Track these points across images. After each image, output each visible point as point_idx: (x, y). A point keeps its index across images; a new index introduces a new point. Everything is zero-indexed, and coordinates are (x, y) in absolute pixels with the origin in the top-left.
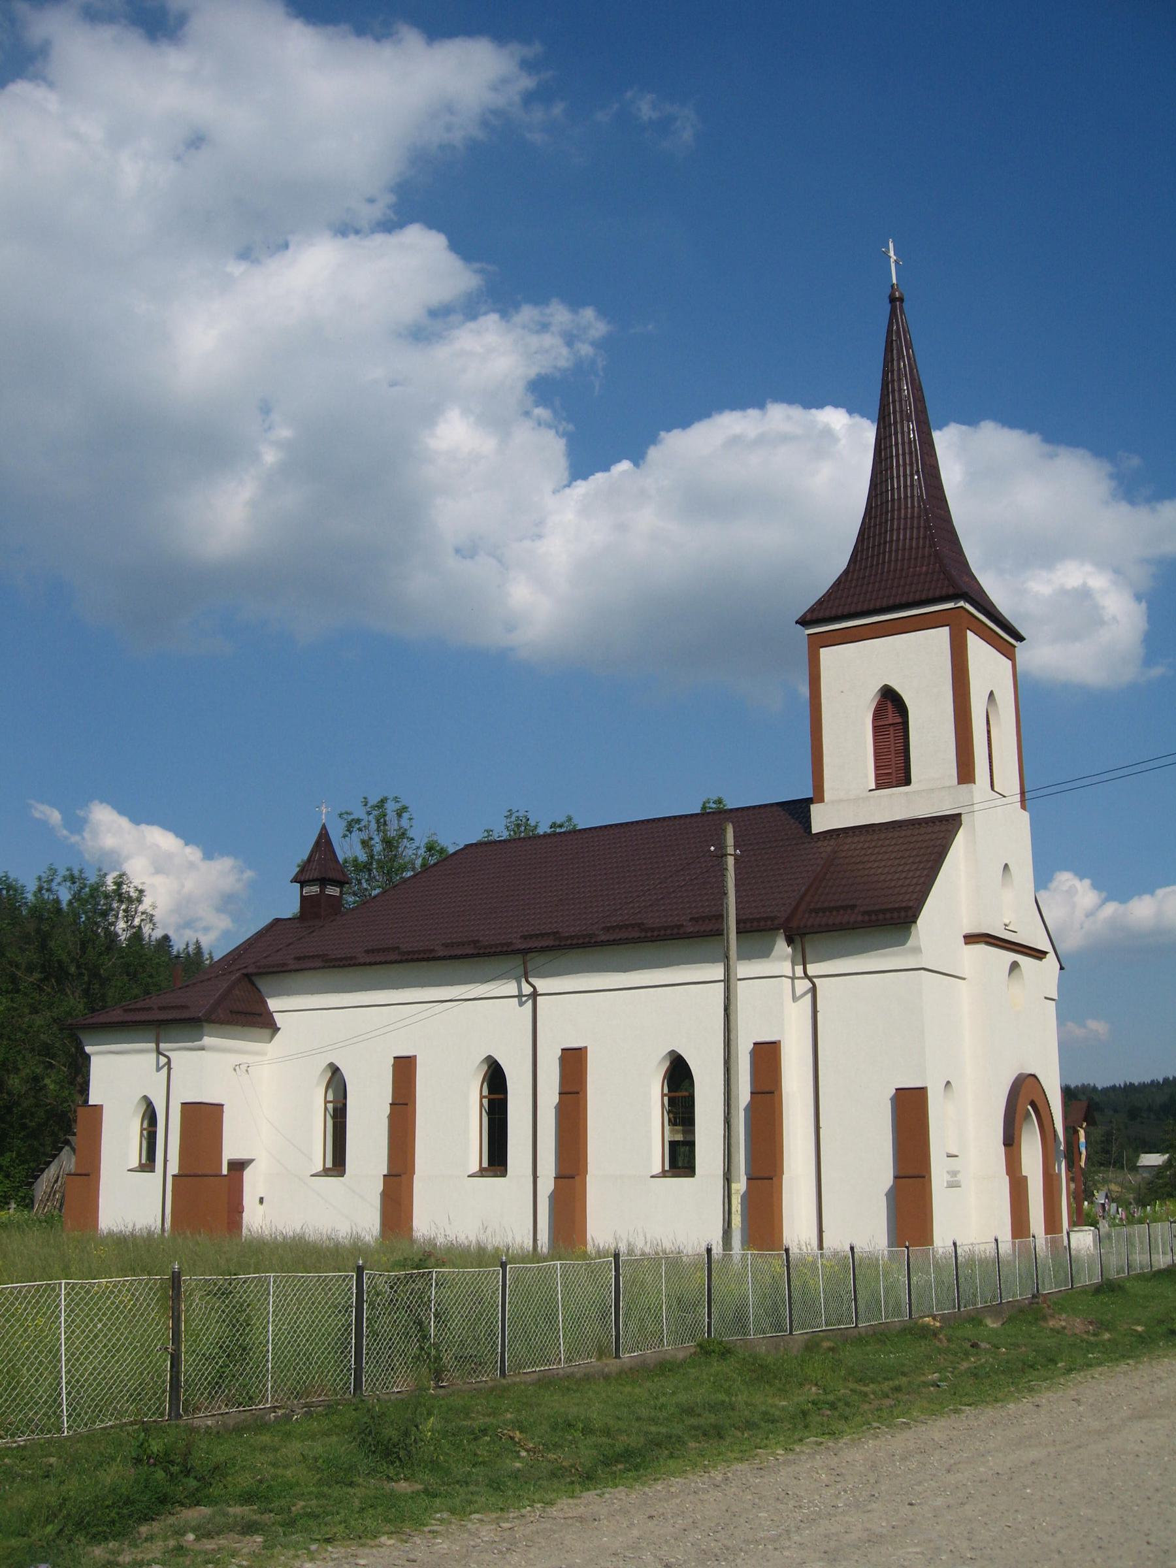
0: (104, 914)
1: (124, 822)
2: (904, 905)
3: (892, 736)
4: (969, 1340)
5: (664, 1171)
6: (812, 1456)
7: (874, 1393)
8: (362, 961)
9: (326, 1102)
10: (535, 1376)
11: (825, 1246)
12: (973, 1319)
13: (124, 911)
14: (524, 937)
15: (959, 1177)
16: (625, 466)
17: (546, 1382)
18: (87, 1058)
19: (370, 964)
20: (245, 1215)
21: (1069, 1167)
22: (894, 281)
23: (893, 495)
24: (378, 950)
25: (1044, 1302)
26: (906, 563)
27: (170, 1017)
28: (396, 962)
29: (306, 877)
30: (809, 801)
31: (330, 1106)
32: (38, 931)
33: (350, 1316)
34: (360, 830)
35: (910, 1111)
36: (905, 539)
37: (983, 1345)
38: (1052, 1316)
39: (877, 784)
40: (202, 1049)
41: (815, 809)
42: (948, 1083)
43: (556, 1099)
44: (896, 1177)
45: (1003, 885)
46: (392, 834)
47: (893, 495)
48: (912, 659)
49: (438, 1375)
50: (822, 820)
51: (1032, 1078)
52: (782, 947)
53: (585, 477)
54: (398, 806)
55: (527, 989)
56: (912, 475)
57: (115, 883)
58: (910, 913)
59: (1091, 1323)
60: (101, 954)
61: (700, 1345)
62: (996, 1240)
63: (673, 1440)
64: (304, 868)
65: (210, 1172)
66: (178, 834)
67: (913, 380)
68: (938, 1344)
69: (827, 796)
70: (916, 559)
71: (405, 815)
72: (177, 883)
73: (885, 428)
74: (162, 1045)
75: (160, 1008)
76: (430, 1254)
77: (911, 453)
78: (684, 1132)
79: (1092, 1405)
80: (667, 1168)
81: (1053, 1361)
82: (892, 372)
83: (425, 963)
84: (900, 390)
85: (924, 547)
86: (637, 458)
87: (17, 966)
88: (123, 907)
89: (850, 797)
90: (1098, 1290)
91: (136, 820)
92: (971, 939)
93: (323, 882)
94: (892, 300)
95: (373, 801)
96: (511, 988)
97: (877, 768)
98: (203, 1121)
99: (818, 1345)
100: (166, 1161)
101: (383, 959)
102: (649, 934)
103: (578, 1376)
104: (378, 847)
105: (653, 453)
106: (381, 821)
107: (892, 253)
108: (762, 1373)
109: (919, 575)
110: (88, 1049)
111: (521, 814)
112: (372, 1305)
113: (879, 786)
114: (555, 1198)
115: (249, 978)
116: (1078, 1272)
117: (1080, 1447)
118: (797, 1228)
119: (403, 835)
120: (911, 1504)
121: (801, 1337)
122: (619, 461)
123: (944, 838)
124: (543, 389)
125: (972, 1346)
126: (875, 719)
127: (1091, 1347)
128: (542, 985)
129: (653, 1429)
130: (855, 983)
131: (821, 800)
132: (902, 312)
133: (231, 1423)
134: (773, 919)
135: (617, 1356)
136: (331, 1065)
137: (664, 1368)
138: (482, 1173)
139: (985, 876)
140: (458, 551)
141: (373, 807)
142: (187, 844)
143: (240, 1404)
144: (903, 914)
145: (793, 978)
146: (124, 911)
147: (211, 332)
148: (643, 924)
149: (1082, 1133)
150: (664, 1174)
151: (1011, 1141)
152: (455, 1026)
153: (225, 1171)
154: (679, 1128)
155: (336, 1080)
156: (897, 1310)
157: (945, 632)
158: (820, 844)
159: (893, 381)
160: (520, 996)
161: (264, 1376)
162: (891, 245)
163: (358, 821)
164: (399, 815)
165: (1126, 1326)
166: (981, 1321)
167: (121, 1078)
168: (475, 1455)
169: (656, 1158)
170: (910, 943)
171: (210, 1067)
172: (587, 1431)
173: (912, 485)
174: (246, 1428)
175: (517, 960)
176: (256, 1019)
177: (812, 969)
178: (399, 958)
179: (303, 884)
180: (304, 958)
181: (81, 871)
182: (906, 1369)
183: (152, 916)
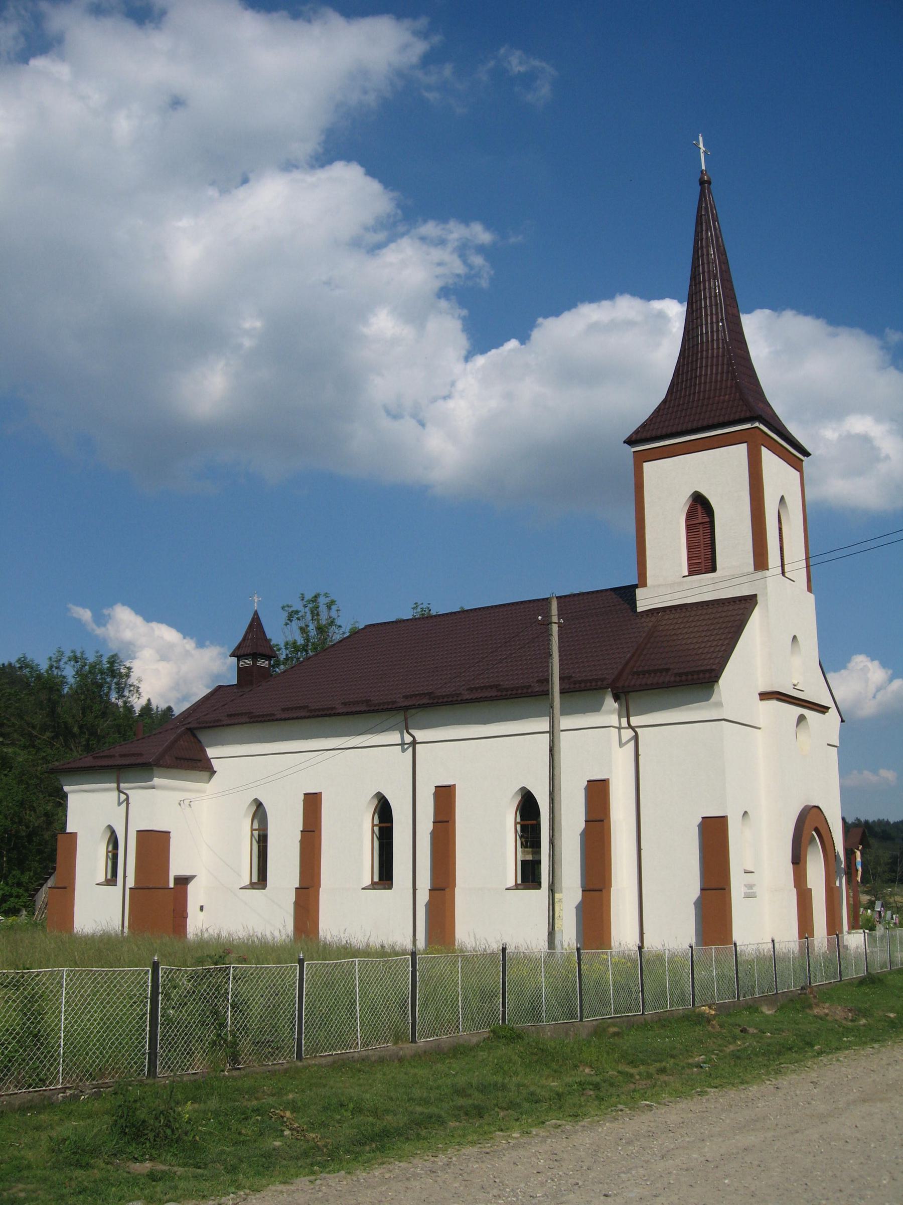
0: (101, 686)
1: (139, 620)
2: (708, 667)
3: (701, 532)
4: (740, 1026)
5: (516, 884)
6: (544, 1140)
7: (640, 1074)
8: (278, 717)
9: (252, 830)
10: (330, 1059)
11: (557, 942)
12: (750, 1007)
13: (116, 684)
14: (406, 697)
15: (755, 889)
16: (513, 344)
17: (341, 1065)
18: (65, 796)
19: (285, 719)
20: (189, 920)
21: (848, 882)
22: (703, 168)
23: (702, 338)
24: (292, 709)
25: (811, 993)
26: (715, 396)
27: (127, 762)
28: (305, 717)
29: (241, 652)
30: (636, 586)
31: (256, 833)
32: (49, 700)
33: (145, 1006)
34: (298, 619)
35: (714, 835)
36: (711, 374)
37: (752, 1030)
38: (817, 1005)
39: (689, 571)
40: (153, 787)
41: (639, 592)
42: (746, 813)
43: (430, 827)
44: (702, 889)
45: (792, 652)
46: (324, 622)
47: (702, 338)
48: (716, 470)
49: (234, 1058)
50: (645, 600)
51: (817, 810)
52: (610, 703)
53: (483, 351)
54: (328, 600)
55: (408, 739)
56: (717, 323)
57: (109, 662)
58: (713, 674)
59: (850, 1010)
60: (96, 717)
61: (493, 1031)
62: (773, 941)
63: (433, 1120)
64: (239, 647)
65: (160, 886)
66: (179, 630)
67: (718, 246)
68: (710, 1029)
69: (649, 581)
70: (721, 389)
71: (334, 607)
72: (167, 666)
73: (695, 285)
74: (122, 785)
75: (121, 756)
76: (228, 952)
77: (716, 305)
78: (533, 853)
79: (827, 1087)
80: (519, 882)
81: (810, 1045)
82: (702, 240)
83: (327, 718)
84: (708, 254)
85: (727, 380)
86: (524, 339)
87: (34, 727)
88: (115, 680)
89: (668, 582)
90: (862, 982)
91: (148, 619)
92: (765, 696)
93: (255, 656)
94: (702, 183)
95: (309, 596)
96: (394, 737)
97: (689, 558)
98: (155, 845)
99: (604, 1030)
100: (125, 877)
101: (295, 715)
102: (504, 693)
103: (373, 1059)
104: (313, 632)
105: (536, 334)
106: (315, 613)
107: (701, 146)
108: (543, 1056)
109: (723, 402)
110: (66, 788)
111: (424, 606)
112: (167, 996)
113: (691, 573)
114: (430, 906)
115: (192, 731)
116: (846, 968)
117: (797, 1132)
118: (623, 933)
119: (332, 623)
120: (606, 1195)
121: (590, 1024)
122: (509, 340)
123: (743, 614)
124: (456, 293)
125: (742, 1031)
126: (687, 520)
127: (848, 1031)
128: (420, 735)
129: (419, 1109)
130: (670, 733)
131: (644, 584)
132: (710, 192)
133: (17, 1103)
134: (602, 680)
135: (414, 1041)
136: (256, 800)
137: (458, 1051)
138: (374, 886)
139: (777, 643)
140: (388, 413)
141: (309, 601)
142: (184, 638)
143: (30, 1086)
144: (707, 675)
145: (620, 728)
146: (116, 684)
147: (193, 247)
148: (499, 685)
149: (858, 854)
150: (517, 887)
151: (798, 860)
152: (351, 770)
153: (172, 885)
154: (530, 850)
155: (259, 811)
156: (682, 999)
157: (743, 447)
158: (643, 620)
159: (702, 248)
160: (402, 744)
161: (55, 1060)
162: (701, 139)
163: (297, 612)
164: (329, 608)
165: (881, 1013)
166: (757, 1009)
167: (91, 811)
168: (240, 1133)
169: (510, 873)
170: (714, 698)
171: (160, 802)
172: (358, 1110)
173: (718, 331)
174: (30, 1108)
175: (400, 717)
176: (196, 764)
177: (635, 721)
178: (308, 714)
179: (239, 658)
180: (234, 715)
181: (82, 653)
182: (674, 1052)
183: (139, 687)
